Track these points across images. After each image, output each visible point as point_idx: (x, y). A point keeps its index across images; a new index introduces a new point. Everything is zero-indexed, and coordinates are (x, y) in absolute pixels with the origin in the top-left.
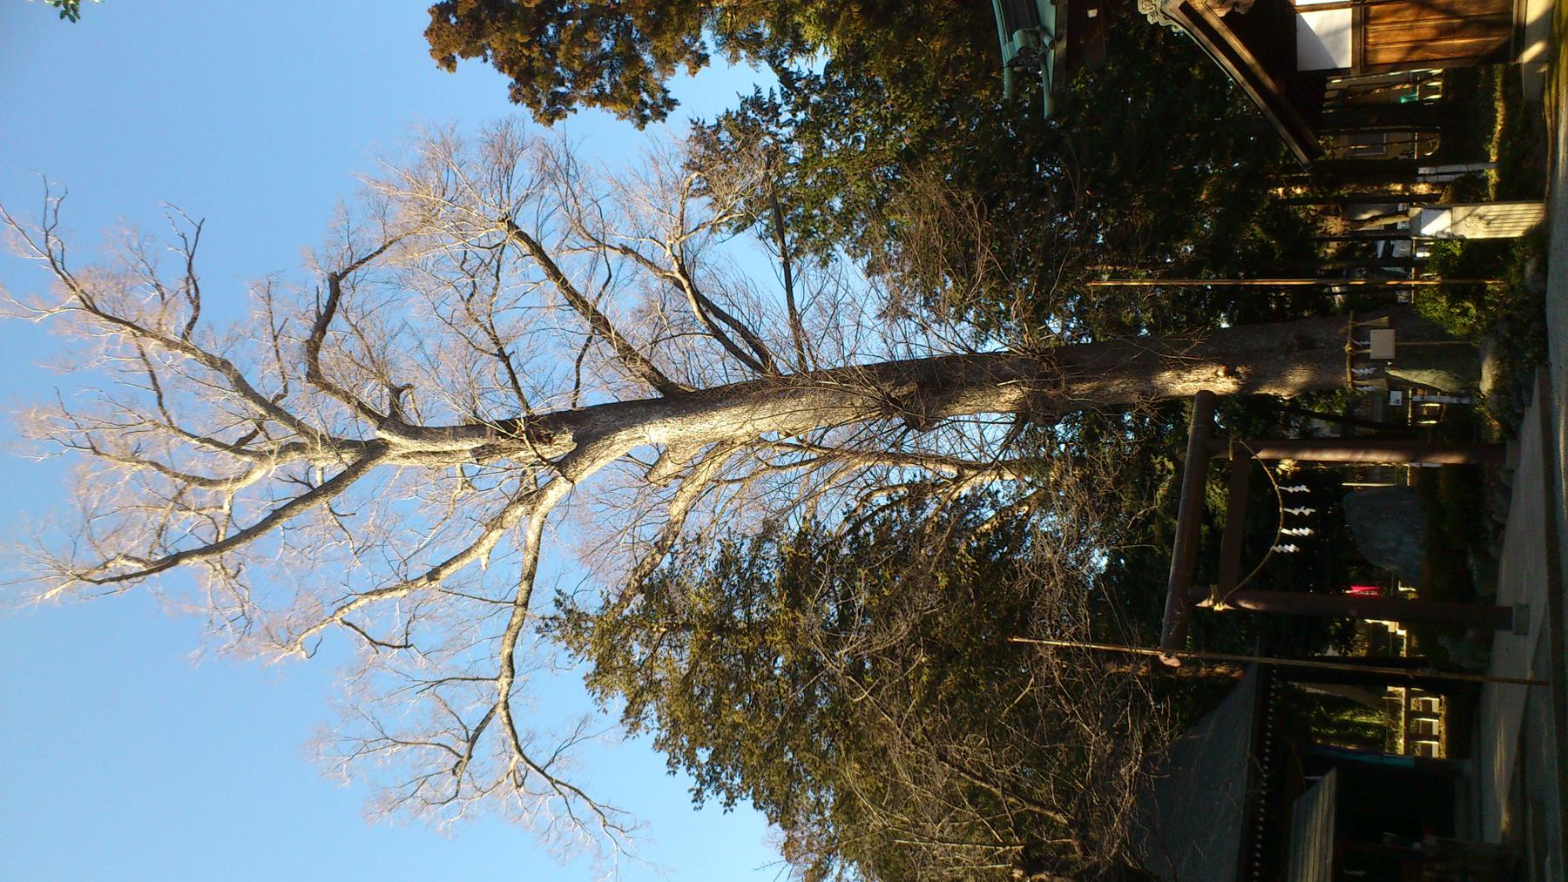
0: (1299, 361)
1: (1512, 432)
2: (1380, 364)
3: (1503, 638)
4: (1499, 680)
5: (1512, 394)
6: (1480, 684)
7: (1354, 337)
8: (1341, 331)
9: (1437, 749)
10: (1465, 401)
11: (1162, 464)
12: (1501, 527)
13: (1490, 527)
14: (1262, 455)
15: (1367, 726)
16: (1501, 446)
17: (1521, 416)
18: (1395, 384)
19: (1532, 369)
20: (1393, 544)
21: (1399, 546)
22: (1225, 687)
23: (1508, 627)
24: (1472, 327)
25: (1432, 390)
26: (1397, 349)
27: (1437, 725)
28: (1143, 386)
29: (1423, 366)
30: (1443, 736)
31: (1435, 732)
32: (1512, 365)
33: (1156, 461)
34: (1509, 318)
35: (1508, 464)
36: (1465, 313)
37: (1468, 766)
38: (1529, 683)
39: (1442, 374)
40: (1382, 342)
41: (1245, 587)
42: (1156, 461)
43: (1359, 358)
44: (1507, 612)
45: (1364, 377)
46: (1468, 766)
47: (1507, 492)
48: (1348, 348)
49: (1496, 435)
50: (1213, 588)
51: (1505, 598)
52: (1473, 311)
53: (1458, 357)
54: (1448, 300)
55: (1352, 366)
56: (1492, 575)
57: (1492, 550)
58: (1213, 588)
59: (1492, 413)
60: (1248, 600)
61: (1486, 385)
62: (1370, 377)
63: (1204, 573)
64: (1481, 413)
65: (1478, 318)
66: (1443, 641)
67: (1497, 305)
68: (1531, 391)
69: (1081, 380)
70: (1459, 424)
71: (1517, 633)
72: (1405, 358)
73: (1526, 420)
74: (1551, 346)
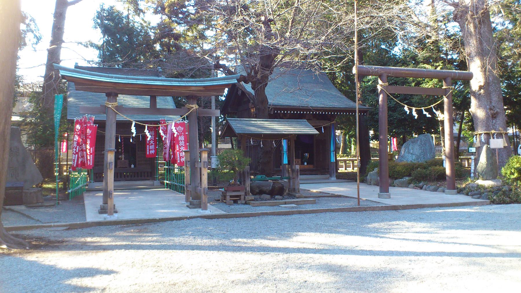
0: (487, 113)
1: (460, 191)
2: (488, 143)
3: (377, 189)
4: (358, 187)
5: (479, 193)
6: (356, 181)
7: (498, 134)
8: (500, 129)
9: (341, 170)
10: (472, 175)
11: (439, 66)
12: (421, 188)
13: (421, 184)
14: (445, 100)
15: (350, 149)
16: (454, 188)
17: (467, 194)
18: (479, 149)
19: (489, 199)
20: (412, 151)
21: (411, 153)
22: (353, 99)
23: (381, 192)
24: (505, 177)
25: (477, 161)
26: (494, 150)
27: (350, 170)
28: (473, 54)
29: (488, 158)
30: (346, 171)
31: (347, 169)
32: (490, 191)
33: (440, 63)
34: (511, 190)
35: (447, 191)
36: (512, 174)
37: (334, 179)
38: (359, 199)
39: (485, 166)
40: (498, 143)
41: (388, 96)
42: (440, 63)
43: (488, 136)
44: (387, 191)
45: (480, 138)
46: (334, 179)
47: (435, 190)
48: (493, 131)
49: (459, 186)
50: (387, 84)
51: (391, 190)
52: (512, 177)
53: (493, 170)
54: (518, 168)
55: (485, 134)
56: (402, 185)
57: (412, 185)
58: (387, 84)
59: (468, 184)
60: (383, 98)
61: (480, 182)
62: (481, 141)
63: (395, 80)
64: (468, 181)
65: (509, 179)
66: (376, 170)
67: (516, 185)
68: (479, 198)
69: (475, 27)
70: (461, 173)
71: (379, 195)
72: (491, 152)
73: (467, 196)
74: (500, 205)
